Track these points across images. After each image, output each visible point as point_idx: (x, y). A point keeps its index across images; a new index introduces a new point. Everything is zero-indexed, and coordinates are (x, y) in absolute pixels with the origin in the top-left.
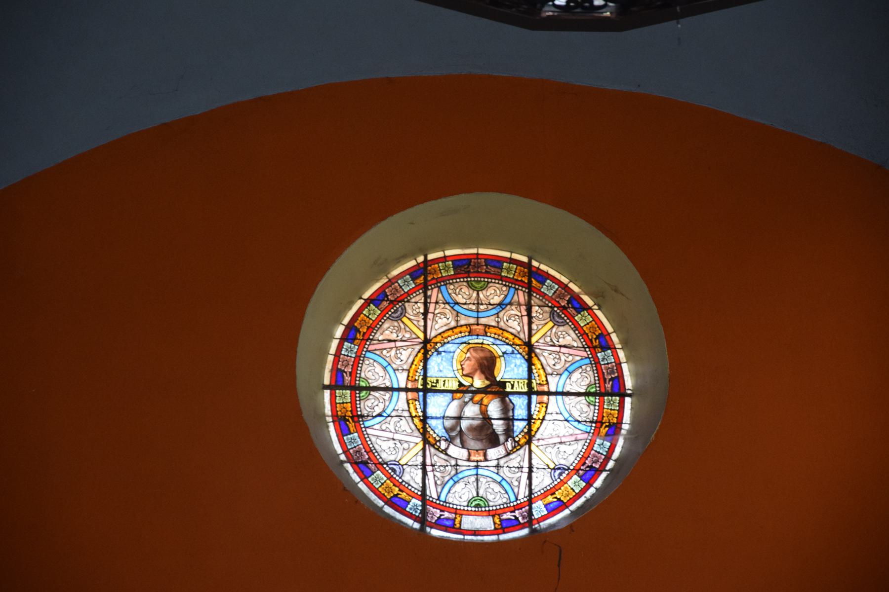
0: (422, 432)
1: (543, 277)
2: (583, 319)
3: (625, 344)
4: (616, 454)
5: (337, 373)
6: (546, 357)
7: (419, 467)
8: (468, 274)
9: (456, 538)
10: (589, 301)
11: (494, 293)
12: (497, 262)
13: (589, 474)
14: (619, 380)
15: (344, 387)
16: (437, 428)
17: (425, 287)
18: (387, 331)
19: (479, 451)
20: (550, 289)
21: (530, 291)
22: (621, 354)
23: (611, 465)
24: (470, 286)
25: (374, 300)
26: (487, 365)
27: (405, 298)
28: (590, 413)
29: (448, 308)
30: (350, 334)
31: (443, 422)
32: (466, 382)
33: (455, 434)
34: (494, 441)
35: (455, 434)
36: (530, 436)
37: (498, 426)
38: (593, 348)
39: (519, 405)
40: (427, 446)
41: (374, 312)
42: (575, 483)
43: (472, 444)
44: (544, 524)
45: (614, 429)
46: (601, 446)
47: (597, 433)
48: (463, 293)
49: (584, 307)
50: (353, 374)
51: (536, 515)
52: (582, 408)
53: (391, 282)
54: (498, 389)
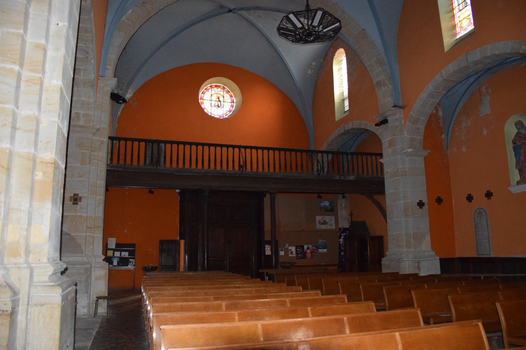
0: (83, 310)
1: (225, 88)
2: (230, 94)
3: (235, 97)
4: (233, 110)
5: (201, 98)
6: (225, 97)
7: (104, 163)
8: (216, 87)
9: (406, 309)
10: (230, 91)
11: (220, 89)
12: (220, 86)
13: (230, 112)
14: (233, 101)
15: (202, 99)
16: (213, 105)
17: (211, 88)
18: (207, 93)
19: (49, 164)
20: (226, 90)
21: (224, 89)
22: (234, 98)
23: (232, 111)
24: (217, 88)
25: (205, 89)
26: (218, 98)
27: (209, 89)
28: (230, 105)
29: (214, 91)
30: (202, 93)
31: (101, 227)
32: (216, 100)
33: (215, 106)
34: (219, 107)
35: (215, 106)
36: (223, 107)
37: (220, 105)
38: (231, 97)
39: (222, 103)
40: (315, 11)
41: (205, 91)
42: (228, 113)
43: (217, 107)
44: (225, 117)
45: (233, 106)
46: (231, 109)
47: (231, 107)
48: (215, 89)
49: (230, 92)
50: (203, 98)
51: (224, 116)
52: (230, 104)
53: (207, 87)
54: (220, 101)
